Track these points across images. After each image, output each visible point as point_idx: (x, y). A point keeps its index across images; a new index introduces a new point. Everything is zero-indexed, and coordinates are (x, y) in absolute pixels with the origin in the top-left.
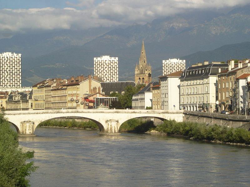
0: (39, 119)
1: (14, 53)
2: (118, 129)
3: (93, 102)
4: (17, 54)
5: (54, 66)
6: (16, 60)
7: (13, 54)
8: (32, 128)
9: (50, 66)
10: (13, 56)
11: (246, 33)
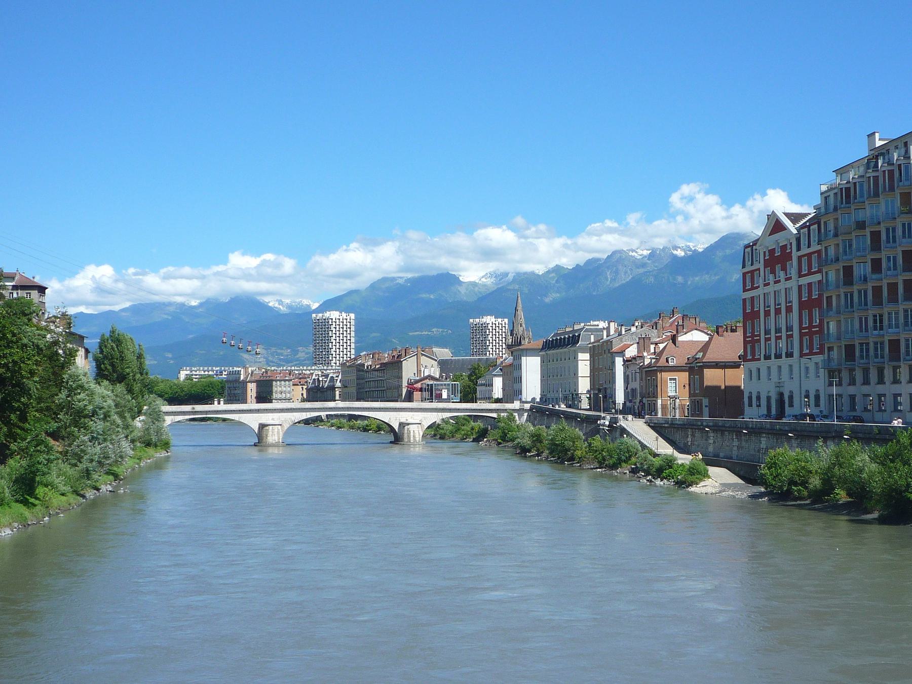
0: (289, 418)
1: (343, 312)
2: (419, 435)
3: (894, 409)
4: (347, 314)
5: (429, 333)
6: (345, 323)
7: (340, 314)
8: (277, 432)
9: (422, 333)
10: (341, 318)
11: (733, 280)
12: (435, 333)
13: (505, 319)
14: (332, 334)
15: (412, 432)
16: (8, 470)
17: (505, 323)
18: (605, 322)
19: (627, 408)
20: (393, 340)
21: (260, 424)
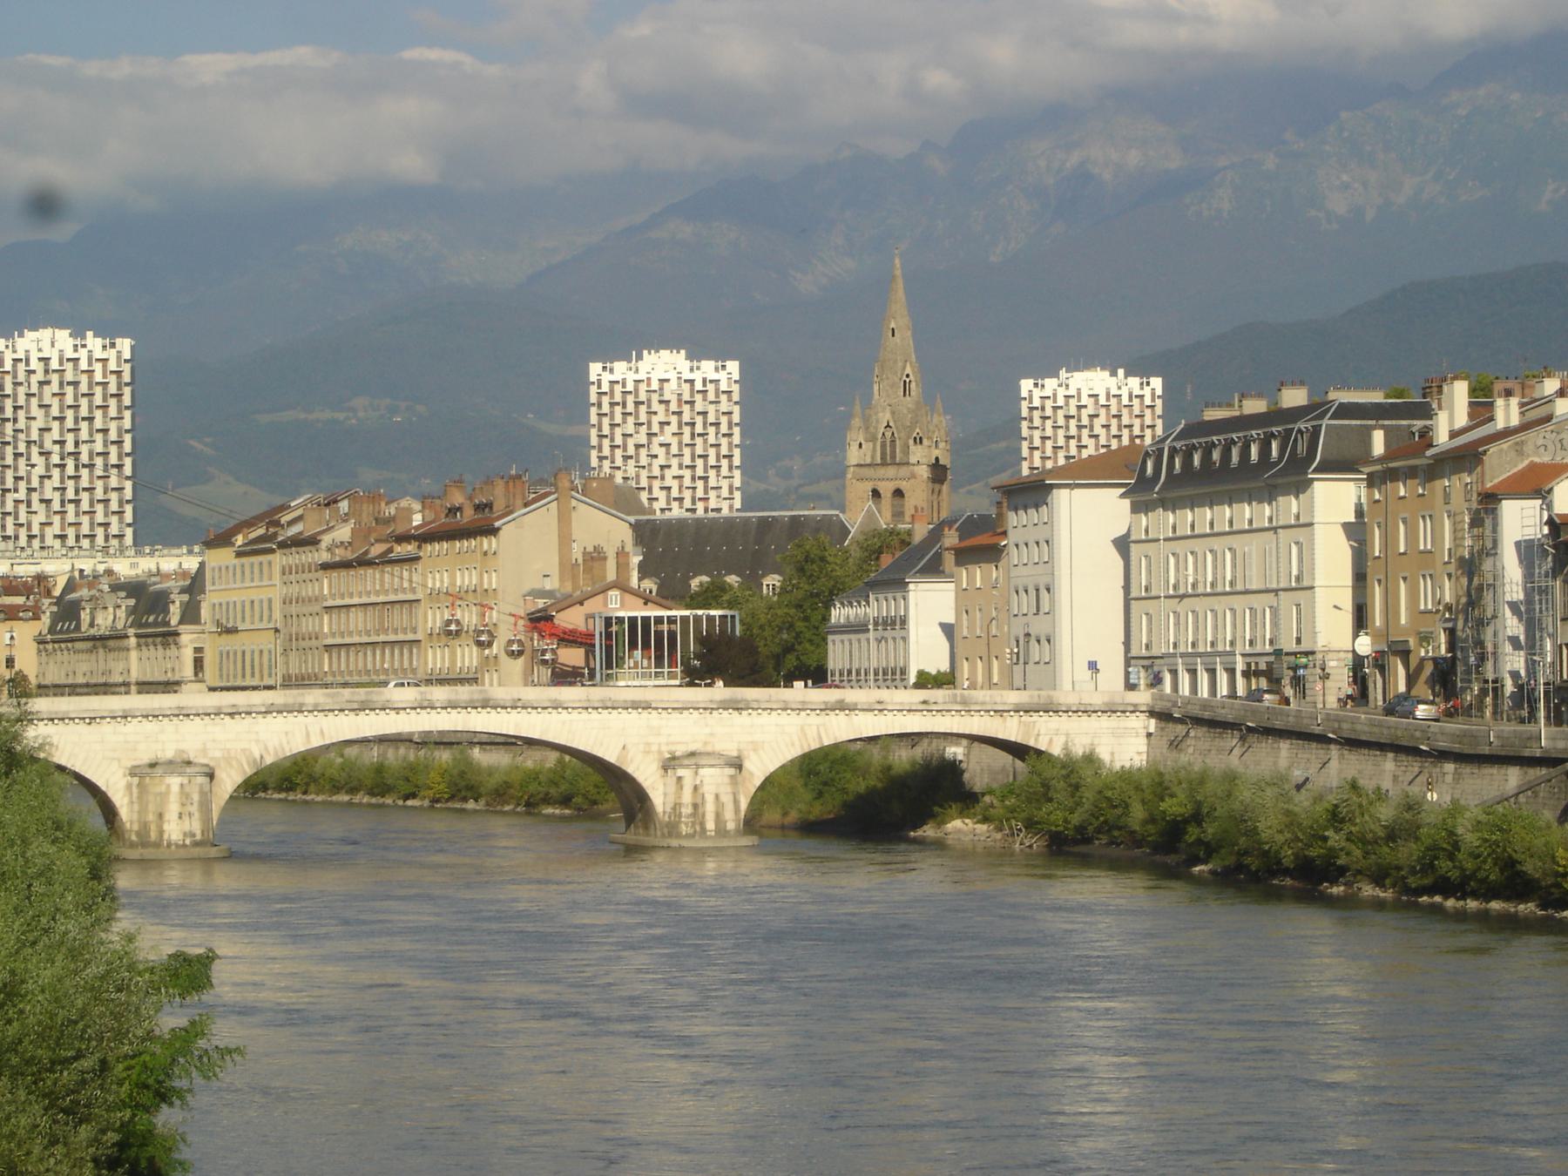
0: (243, 750)
1: (90, 334)
5: (341, 416)
6: (98, 377)
7: (78, 342)
12: (361, 414)
13: (118, 341)
14: (706, 450)
15: (710, 799)
16: (134, 998)
17: (1153, 394)
18: (1114, 374)
19: (672, 664)
20: (193, 443)
21: (133, 771)
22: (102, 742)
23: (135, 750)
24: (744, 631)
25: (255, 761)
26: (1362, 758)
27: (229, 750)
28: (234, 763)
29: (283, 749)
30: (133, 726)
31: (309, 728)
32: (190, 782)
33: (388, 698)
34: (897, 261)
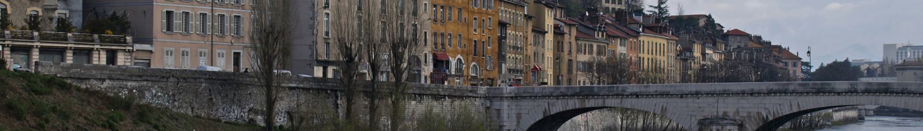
22: (688, 107)
23: (703, 111)
24: (388, 99)
25: (763, 118)
26: (739, 98)
27: (750, 113)
28: (753, 119)
29: (778, 113)
30: (703, 101)
31: (792, 102)
32: (722, 128)
33: (834, 87)
34: (595, 68)
